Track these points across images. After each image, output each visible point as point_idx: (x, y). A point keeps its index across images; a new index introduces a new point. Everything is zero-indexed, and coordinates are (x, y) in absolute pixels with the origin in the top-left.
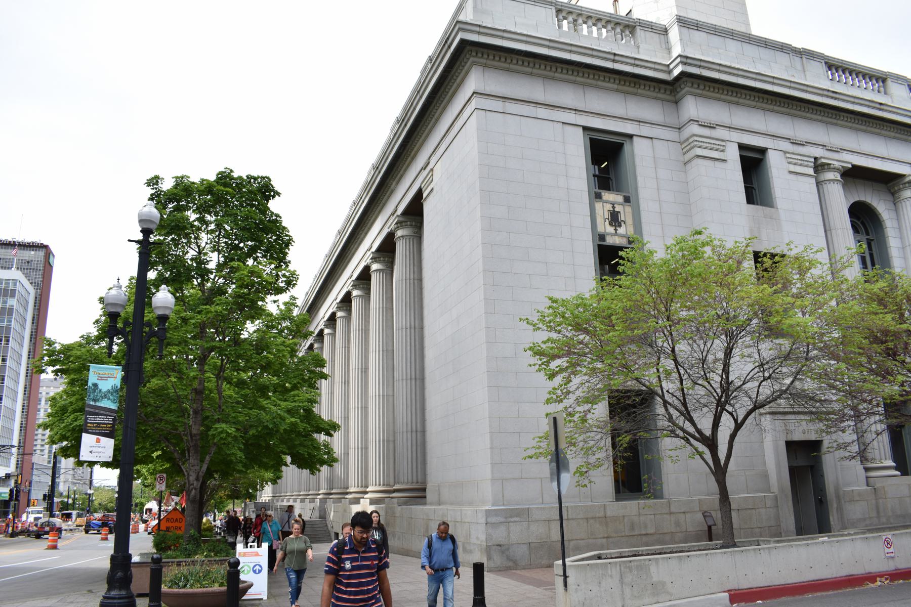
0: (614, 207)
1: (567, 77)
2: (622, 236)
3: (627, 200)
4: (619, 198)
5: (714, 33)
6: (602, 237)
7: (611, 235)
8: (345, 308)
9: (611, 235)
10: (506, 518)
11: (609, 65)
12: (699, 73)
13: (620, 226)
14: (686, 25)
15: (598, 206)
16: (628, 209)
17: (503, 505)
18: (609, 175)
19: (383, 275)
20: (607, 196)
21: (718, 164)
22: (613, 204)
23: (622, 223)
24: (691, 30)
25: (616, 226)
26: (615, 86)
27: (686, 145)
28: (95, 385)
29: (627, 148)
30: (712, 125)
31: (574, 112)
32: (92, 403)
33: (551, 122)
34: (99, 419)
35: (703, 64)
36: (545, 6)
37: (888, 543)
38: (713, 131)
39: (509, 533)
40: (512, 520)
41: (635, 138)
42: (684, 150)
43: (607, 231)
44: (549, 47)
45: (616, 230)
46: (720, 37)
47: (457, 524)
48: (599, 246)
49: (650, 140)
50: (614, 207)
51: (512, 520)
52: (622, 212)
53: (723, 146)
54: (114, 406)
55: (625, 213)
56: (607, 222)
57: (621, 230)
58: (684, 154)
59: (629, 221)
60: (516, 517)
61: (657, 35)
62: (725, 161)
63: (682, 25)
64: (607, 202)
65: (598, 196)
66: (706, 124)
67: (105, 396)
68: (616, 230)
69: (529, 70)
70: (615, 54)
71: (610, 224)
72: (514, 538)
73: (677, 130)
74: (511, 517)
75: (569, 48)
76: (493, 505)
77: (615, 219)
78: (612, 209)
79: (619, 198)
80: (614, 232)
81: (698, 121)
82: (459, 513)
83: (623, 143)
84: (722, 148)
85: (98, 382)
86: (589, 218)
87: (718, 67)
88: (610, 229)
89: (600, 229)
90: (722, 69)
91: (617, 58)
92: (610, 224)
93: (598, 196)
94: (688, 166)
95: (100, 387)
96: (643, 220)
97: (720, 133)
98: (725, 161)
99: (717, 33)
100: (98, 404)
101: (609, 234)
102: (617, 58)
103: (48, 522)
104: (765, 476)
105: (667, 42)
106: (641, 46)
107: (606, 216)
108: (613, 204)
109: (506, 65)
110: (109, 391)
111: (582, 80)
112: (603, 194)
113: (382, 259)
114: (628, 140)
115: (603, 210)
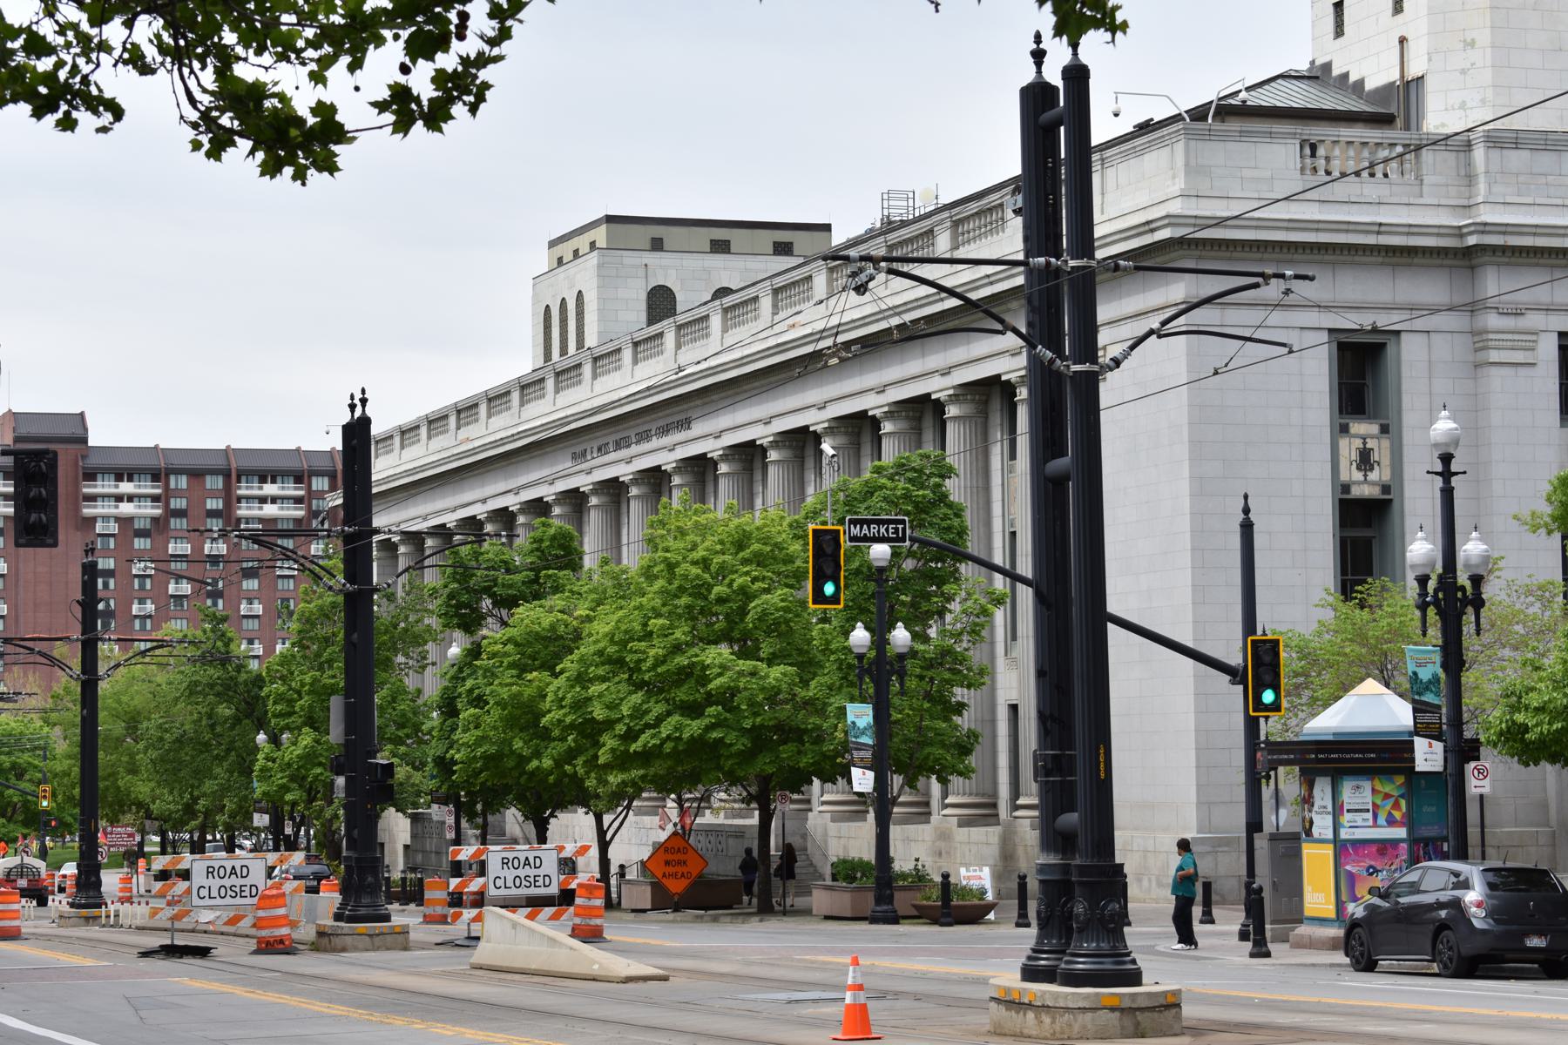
0: (1365, 443)
1: (1311, 257)
2: (1373, 484)
3: (1385, 429)
4: (1374, 429)
5: (1544, 147)
6: (1346, 488)
7: (1358, 483)
8: (843, 429)
9: (1372, 437)
10: (1213, 847)
11: (1371, 240)
12: (1502, 243)
13: (1372, 469)
14: (1497, 145)
15: (1344, 443)
16: (1386, 443)
17: (1210, 833)
18: (1364, 379)
19: (964, 429)
20: (1359, 427)
21: (1522, 371)
22: (1364, 439)
23: (1376, 465)
24: (1505, 151)
25: (1365, 470)
26: (1380, 259)
27: (1479, 339)
28: (853, 723)
29: (1390, 350)
30: (1519, 311)
31: (1317, 309)
32: (854, 740)
33: (1285, 330)
34: (863, 754)
35: (1509, 229)
36: (1284, 141)
37: (864, 774)
38: (1520, 319)
39: (1216, 865)
40: (1220, 849)
41: (1404, 336)
42: (1477, 345)
43: (1353, 479)
44: (1287, 229)
45: (1365, 476)
46: (1553, 153)
47: (1149, 854)
48: (1341, 501)
49: (1426, 334)
50: (1365, 443)
51: (1220, 849)
52: (1376, 450)
53: (1534, 341)
54: (870, 742)
55: (1381, 450)
56: (1354, 464)
57: (1373, 476)
58: (1476, 350)
59: (1386, 462)
60: (1225, 846)
61: (1454, 154)
62: (1533, 365)
63: (1492, 145)
64: (1357, 436)
65: (1344, 429)
66: (1510, 311)
67: (863, 733)
68: (1365, 476)
69: (1259, 255)
70: (1380, 224)
71: (1358, 468)
72: (1222, 871)
73: (1469, 314)
74: (1219, 846)
75: (1316, 226)
76: (1198, 833)
77: (1365, 460)
78: (1362, 446)
79: (1374, 429)
80: (1362, 478)
81: (1497, 308)
82: (1152, 842)
83: (1385, 344)
84: (1531, 344)
85: (856, 720)
86: (1329, 466)
87: (1533, 230)
88: (1358, 476)
89: (1344, 476)
90: (1539, 230)
91: (1383, 229)
92: (1359, 468)
93: (1344, 429)
94: (1479, 370)
95: (858, 724)
96: (1406, 459)
97: (1533, 320)
98: (1533, 365)
99: (1549, 147)
100: (859, 740)
101: (1355, 483)
102: (1383, 229)
103: (22, 866)
104: (1544, 806)
105: (1469, 164)
106: (1427, 179)
107: (1354, 458)
108: (1364, 439)
109: (1228, 254)
110: (865, 728)
111: (1331, 258)
112: (1351, 425)
113: (969, 397)
114: (1393, 338)
115: (1349, 449)
